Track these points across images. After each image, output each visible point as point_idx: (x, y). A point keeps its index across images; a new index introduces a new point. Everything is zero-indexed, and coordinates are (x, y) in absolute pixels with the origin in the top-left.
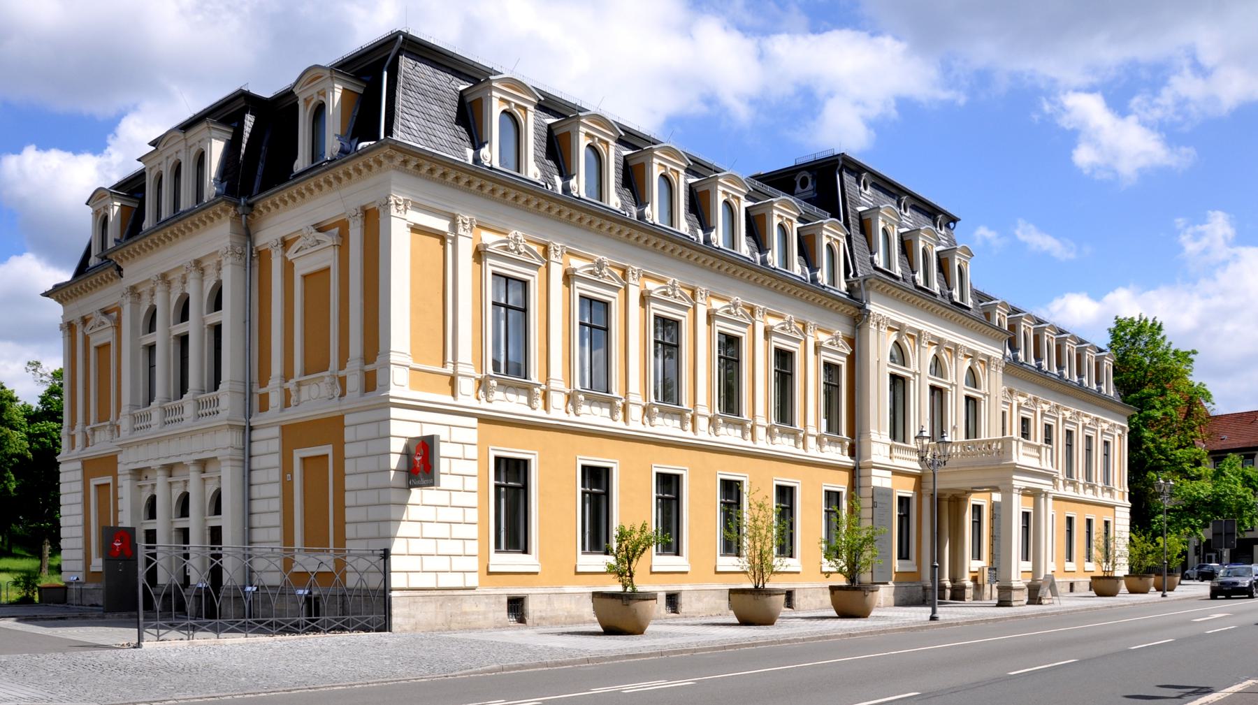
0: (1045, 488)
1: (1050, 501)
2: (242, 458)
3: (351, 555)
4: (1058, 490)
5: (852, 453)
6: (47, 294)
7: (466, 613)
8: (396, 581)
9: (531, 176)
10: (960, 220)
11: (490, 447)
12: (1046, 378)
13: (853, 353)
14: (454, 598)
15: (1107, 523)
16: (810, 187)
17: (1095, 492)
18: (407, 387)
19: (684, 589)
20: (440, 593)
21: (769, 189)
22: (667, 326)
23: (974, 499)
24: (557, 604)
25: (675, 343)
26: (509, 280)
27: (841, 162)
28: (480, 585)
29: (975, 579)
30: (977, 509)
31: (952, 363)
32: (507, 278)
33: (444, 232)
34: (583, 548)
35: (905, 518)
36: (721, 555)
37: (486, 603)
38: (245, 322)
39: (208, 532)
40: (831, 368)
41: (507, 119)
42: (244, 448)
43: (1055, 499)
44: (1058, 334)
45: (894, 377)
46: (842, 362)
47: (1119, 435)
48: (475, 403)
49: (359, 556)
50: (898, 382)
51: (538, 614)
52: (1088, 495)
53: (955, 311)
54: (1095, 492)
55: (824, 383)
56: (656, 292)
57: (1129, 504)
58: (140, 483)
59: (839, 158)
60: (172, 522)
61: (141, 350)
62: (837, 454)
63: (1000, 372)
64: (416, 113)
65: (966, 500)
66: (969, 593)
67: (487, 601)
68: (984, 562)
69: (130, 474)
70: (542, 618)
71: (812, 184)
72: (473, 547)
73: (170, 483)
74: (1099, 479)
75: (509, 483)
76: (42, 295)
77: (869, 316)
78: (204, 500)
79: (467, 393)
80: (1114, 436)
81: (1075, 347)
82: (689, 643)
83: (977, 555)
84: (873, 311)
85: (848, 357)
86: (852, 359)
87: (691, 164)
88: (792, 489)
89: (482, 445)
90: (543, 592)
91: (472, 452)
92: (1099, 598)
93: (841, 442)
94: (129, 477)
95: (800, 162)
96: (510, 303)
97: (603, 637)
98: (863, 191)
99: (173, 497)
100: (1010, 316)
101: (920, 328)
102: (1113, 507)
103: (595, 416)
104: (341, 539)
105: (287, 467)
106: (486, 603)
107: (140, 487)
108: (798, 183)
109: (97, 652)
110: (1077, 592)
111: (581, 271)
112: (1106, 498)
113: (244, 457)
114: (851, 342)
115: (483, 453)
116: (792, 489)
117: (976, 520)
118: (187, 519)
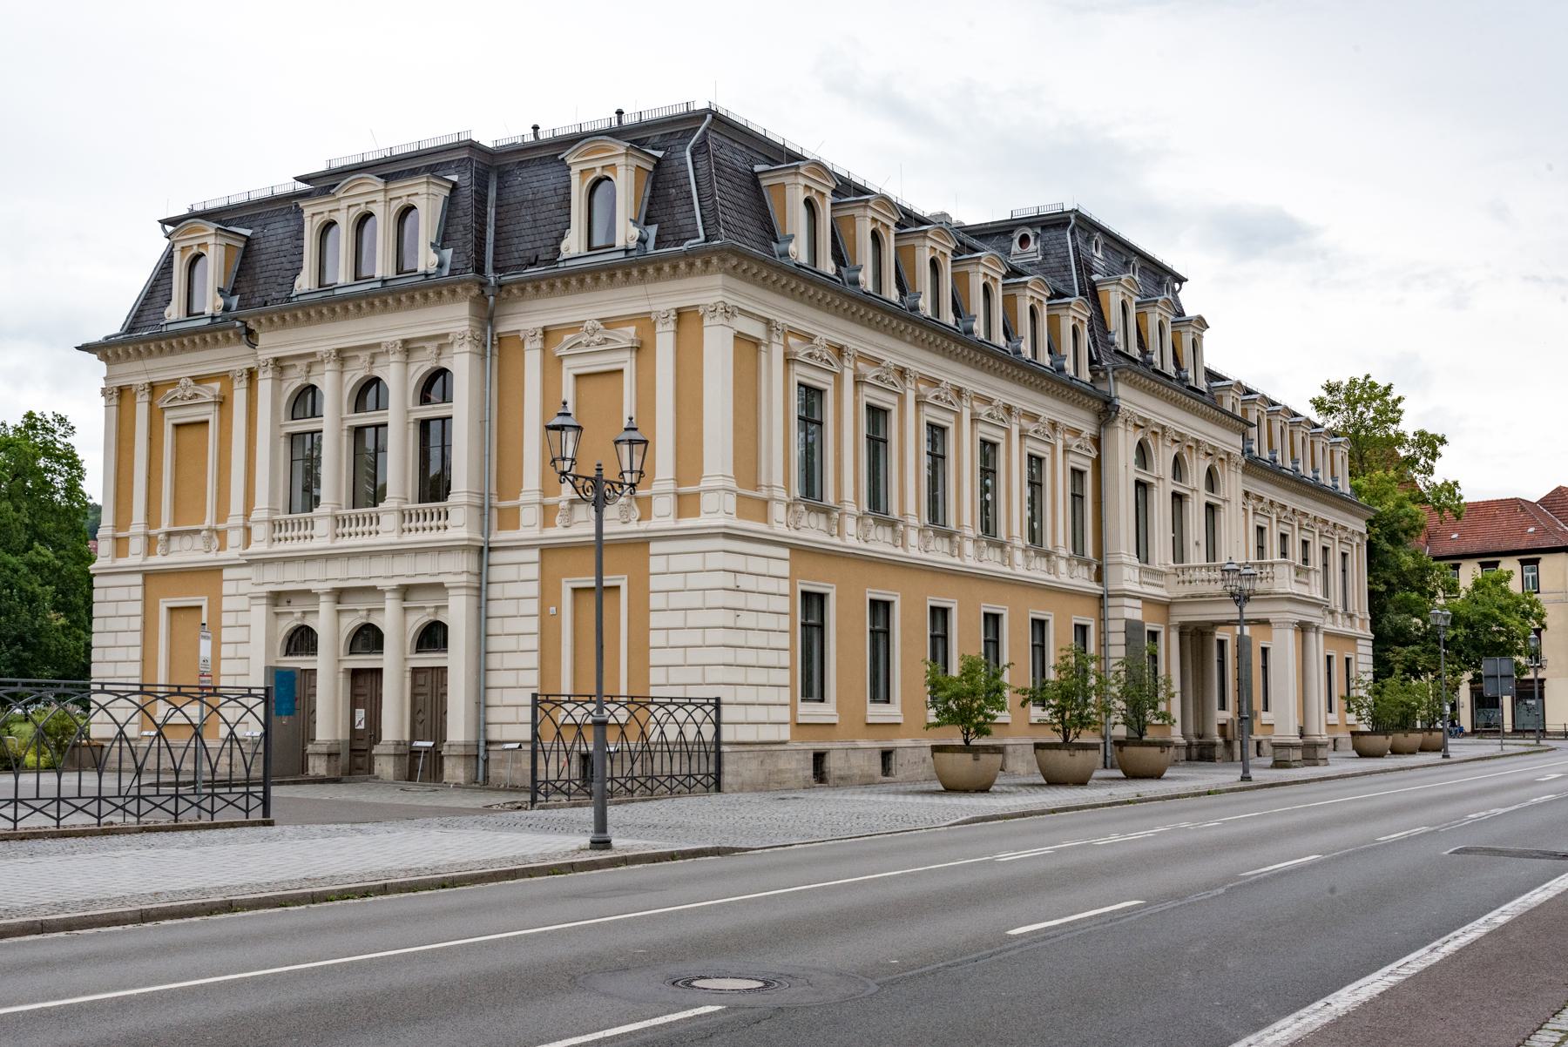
0: (1316, 621)
1: (1321, 636)
2: (477, 585)
3: (103, 691)
4: (1013, 568)
5: (1099, 577)
6: (85, 348)
7: (780, 771)
8: (727, 734)
10: (1186, 280)
11: (867, 590)
12: (1071, 387)
13: (1099, 456)
14: (772, 754)
15: (1348, 660)
16: (1032, 246)
17: (1052, 569)
19: (898, 745)
20: (758, 748)
21: (975, 243)
22: (811, 395)
23: (1220, 634)
24: (853, 761)
27: (1073, 221)
28: (792, 738)
29: (1223, 734)
30: (1222, 643)
33: (759, 339)
35: (881, 637)
36: (803, 700)
37: (797, 760)
38: (482, 422)
39: (408, 675)
40: (1077, 474)
42: (481, 574)
43: (1326, 634)
44: (1244, 395)
45: (1138, 483)
46: (1086, 465)
47: (1358, 545)
49: (662, 705)
50: (1142, 487)
51: (837, 773)
54: (1052, 569)
55: (868, 437)
56: (801, 355)
57: (1372, 636)
58: (278, 610)
59: (1072, 216)
60: (406, 659)
61: (283, 439)
62: (1082, 579)
63: (1240, 471)
64: (729, 205)
65: (1212, 634)
66: (1219, 752)
67: (797, 757)
68: (1228, 715)
69: (267, 597)
70: (841, 778)
71: (1035, 243)
72: (785, 696)
73: (339, 612)
76: (77, 348)
77: (1117, 412)
78: (404, 635)
80: (1352, 547)
81: (1240, 398)
82: (436, 867)
83: (1223, 707)
84: (1122, 406)
85: (1093, 460)
86: (1098, 464)
87: (903, 217)
88: (822, 597)
91: (785, 587)
92: (1361, 759)
93: (1088, 564)
94: (264, 601)
97: (1046, 789)
99: (341, 630)
100: (1051, 302)
101: (1164, 424)
105: (547, 595)
106: (797, 760)
107: (277, 614)
109: (1031, 782)
110: (1341, 750)
113: (481, 583)
114: (1097, 441)
115: (793, 587)
116: (822, 597)
117: (991, 637)
118: (379, 657)
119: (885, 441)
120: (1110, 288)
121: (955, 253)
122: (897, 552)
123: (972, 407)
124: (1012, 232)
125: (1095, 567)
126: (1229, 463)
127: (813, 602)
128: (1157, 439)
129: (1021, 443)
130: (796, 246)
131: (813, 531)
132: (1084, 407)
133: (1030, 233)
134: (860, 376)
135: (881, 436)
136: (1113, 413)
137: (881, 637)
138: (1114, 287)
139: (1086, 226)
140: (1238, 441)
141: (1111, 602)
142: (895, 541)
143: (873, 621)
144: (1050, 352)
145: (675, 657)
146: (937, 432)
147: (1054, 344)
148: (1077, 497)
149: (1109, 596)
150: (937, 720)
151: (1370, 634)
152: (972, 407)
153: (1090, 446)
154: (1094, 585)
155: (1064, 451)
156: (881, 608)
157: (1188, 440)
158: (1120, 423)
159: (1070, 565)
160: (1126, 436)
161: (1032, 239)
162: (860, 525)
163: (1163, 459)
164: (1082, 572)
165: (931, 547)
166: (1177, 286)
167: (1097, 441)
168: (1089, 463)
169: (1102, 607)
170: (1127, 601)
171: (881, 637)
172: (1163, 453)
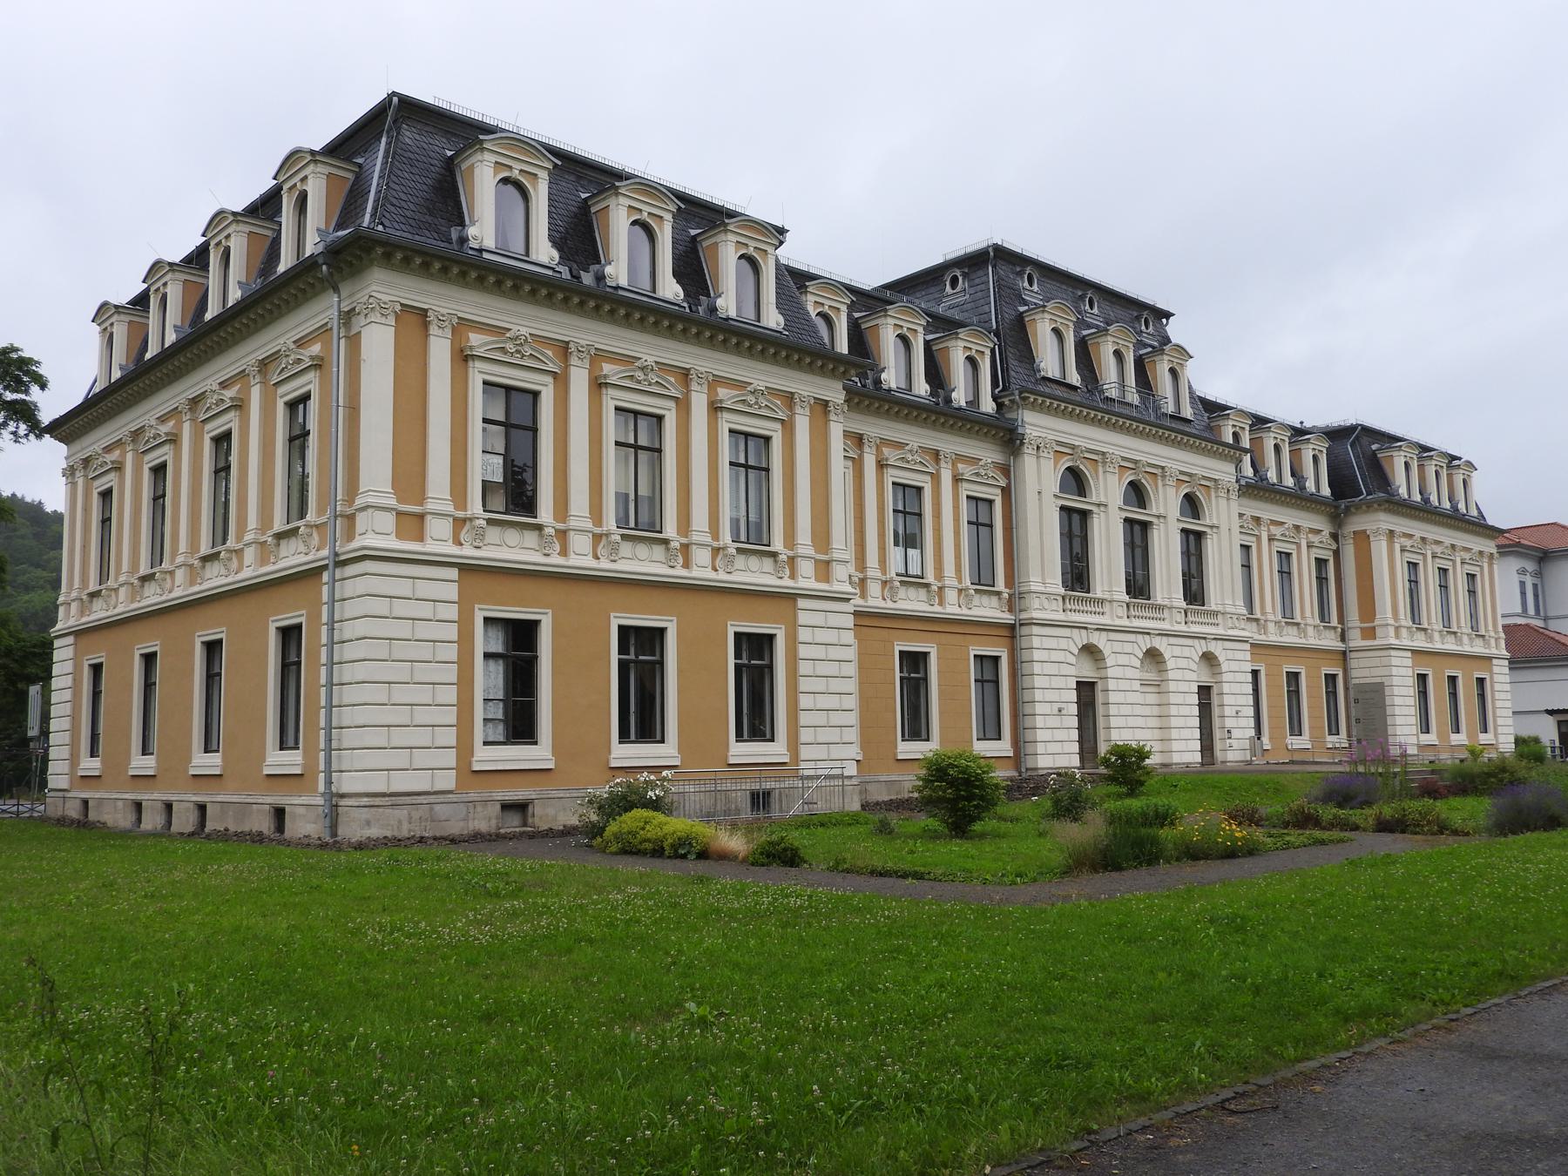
5: (1343, 638)
9: (772, 325)
13: (1338, 548)
17: (1430, 639)
18: (813, 580)
22: (1285, 556)
25: (657, 446)
26: (749, 438)
31: (1157, 491)
32: (747, 435)
34: (903, 735)
40: (1321, 563)
41: (744, 263)
48: (455, 550)
52: (1450, 645)
53: (1171, 428)
57: (1508, 655)
59: (990, 250)
63: (1234, 496)
74: (1308, 613)
75: (641, 657)
79: (438, 540)
89: (465, 604)
90: (357, 804)
95: (950, 256)
96: (640, 443)
98: (1090, 311)
102: (791, 597)
103: (643, 562)
104: (1495, 729)
108: (948, 283)
111: (482, 350)
112: (1478, 648)
114: (1335, 537)
119: (1327, 579)
120: (1037, 317)
121: (1251, 426)
122: (936, 610)
123: (1269, 530)
124: (943, 276)
125: (1339, 630)
126: (1217, 489)
127: (1422, 678)
128: (1097, 466)
129: (1270, 545)
130: (888, 375)
131: (1420, 642)
132: (1317, 512)
133: (958, 273)
134: (959, 474)
135: (1324, 576)
136: (1018, 442)
137: (1294, 694)
138: (1040, 315)
139: (999, 256)
140: (1231, 468)
141: (1353, 655)
142: (1259, 631)
143: (1289, 685)
144: (1293, 475)
145: (820, 718)
146: (1285, 556)
147: (1296, 467)
148: (1322, 580)
149: (1021, 625)
150: (1103, 749)
151: (1505, 652)
152: (1269, 530)
153: (1331, 541)
154: (1340, 644)
155: (1269, 540)
156: (1293, 677)
157: (1199, 479)
158: (1028, 450)
159: (1441, 636)
160: (1228, 505)
161: (960, 279)
162: (963, 595)
163: (1165, 498)
164: (1331, 634)
165: (1285, 633)
166: (1164, 321)
167: (1006, 470)
168: (999, 491)
169: (1013, 637)
170: (1393, 653)
171: (1294, 694)
172: (1105, 479)
